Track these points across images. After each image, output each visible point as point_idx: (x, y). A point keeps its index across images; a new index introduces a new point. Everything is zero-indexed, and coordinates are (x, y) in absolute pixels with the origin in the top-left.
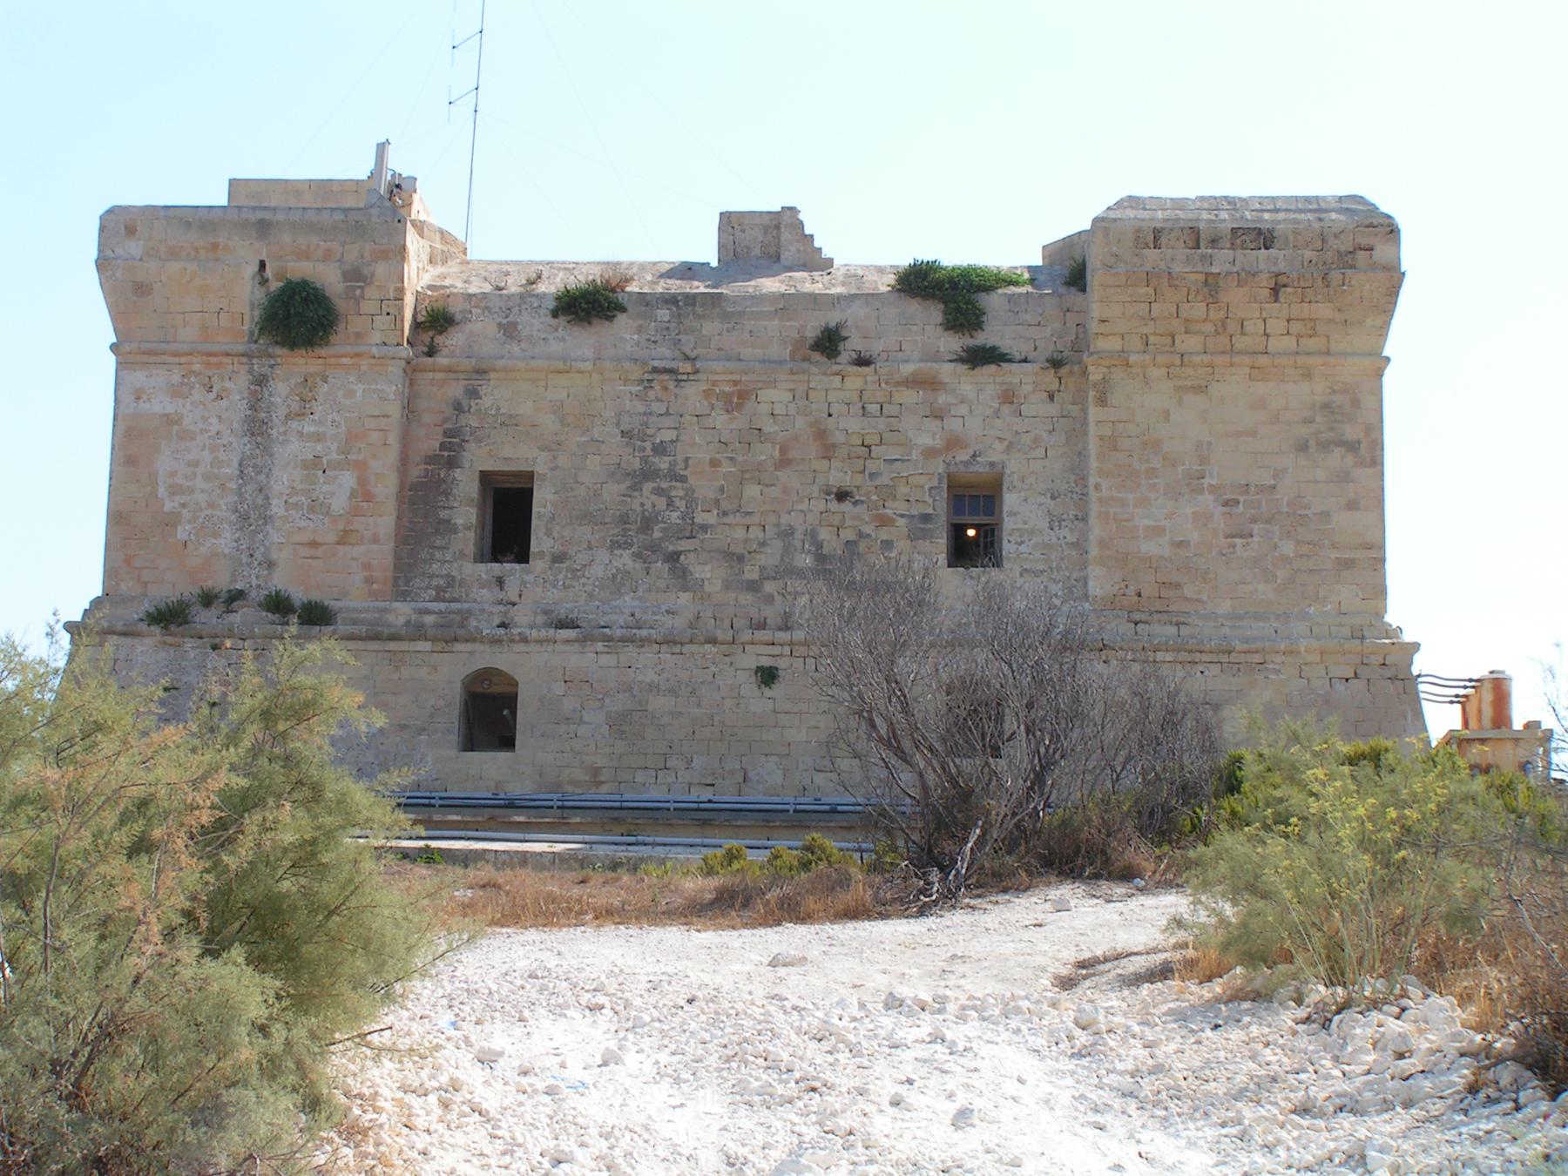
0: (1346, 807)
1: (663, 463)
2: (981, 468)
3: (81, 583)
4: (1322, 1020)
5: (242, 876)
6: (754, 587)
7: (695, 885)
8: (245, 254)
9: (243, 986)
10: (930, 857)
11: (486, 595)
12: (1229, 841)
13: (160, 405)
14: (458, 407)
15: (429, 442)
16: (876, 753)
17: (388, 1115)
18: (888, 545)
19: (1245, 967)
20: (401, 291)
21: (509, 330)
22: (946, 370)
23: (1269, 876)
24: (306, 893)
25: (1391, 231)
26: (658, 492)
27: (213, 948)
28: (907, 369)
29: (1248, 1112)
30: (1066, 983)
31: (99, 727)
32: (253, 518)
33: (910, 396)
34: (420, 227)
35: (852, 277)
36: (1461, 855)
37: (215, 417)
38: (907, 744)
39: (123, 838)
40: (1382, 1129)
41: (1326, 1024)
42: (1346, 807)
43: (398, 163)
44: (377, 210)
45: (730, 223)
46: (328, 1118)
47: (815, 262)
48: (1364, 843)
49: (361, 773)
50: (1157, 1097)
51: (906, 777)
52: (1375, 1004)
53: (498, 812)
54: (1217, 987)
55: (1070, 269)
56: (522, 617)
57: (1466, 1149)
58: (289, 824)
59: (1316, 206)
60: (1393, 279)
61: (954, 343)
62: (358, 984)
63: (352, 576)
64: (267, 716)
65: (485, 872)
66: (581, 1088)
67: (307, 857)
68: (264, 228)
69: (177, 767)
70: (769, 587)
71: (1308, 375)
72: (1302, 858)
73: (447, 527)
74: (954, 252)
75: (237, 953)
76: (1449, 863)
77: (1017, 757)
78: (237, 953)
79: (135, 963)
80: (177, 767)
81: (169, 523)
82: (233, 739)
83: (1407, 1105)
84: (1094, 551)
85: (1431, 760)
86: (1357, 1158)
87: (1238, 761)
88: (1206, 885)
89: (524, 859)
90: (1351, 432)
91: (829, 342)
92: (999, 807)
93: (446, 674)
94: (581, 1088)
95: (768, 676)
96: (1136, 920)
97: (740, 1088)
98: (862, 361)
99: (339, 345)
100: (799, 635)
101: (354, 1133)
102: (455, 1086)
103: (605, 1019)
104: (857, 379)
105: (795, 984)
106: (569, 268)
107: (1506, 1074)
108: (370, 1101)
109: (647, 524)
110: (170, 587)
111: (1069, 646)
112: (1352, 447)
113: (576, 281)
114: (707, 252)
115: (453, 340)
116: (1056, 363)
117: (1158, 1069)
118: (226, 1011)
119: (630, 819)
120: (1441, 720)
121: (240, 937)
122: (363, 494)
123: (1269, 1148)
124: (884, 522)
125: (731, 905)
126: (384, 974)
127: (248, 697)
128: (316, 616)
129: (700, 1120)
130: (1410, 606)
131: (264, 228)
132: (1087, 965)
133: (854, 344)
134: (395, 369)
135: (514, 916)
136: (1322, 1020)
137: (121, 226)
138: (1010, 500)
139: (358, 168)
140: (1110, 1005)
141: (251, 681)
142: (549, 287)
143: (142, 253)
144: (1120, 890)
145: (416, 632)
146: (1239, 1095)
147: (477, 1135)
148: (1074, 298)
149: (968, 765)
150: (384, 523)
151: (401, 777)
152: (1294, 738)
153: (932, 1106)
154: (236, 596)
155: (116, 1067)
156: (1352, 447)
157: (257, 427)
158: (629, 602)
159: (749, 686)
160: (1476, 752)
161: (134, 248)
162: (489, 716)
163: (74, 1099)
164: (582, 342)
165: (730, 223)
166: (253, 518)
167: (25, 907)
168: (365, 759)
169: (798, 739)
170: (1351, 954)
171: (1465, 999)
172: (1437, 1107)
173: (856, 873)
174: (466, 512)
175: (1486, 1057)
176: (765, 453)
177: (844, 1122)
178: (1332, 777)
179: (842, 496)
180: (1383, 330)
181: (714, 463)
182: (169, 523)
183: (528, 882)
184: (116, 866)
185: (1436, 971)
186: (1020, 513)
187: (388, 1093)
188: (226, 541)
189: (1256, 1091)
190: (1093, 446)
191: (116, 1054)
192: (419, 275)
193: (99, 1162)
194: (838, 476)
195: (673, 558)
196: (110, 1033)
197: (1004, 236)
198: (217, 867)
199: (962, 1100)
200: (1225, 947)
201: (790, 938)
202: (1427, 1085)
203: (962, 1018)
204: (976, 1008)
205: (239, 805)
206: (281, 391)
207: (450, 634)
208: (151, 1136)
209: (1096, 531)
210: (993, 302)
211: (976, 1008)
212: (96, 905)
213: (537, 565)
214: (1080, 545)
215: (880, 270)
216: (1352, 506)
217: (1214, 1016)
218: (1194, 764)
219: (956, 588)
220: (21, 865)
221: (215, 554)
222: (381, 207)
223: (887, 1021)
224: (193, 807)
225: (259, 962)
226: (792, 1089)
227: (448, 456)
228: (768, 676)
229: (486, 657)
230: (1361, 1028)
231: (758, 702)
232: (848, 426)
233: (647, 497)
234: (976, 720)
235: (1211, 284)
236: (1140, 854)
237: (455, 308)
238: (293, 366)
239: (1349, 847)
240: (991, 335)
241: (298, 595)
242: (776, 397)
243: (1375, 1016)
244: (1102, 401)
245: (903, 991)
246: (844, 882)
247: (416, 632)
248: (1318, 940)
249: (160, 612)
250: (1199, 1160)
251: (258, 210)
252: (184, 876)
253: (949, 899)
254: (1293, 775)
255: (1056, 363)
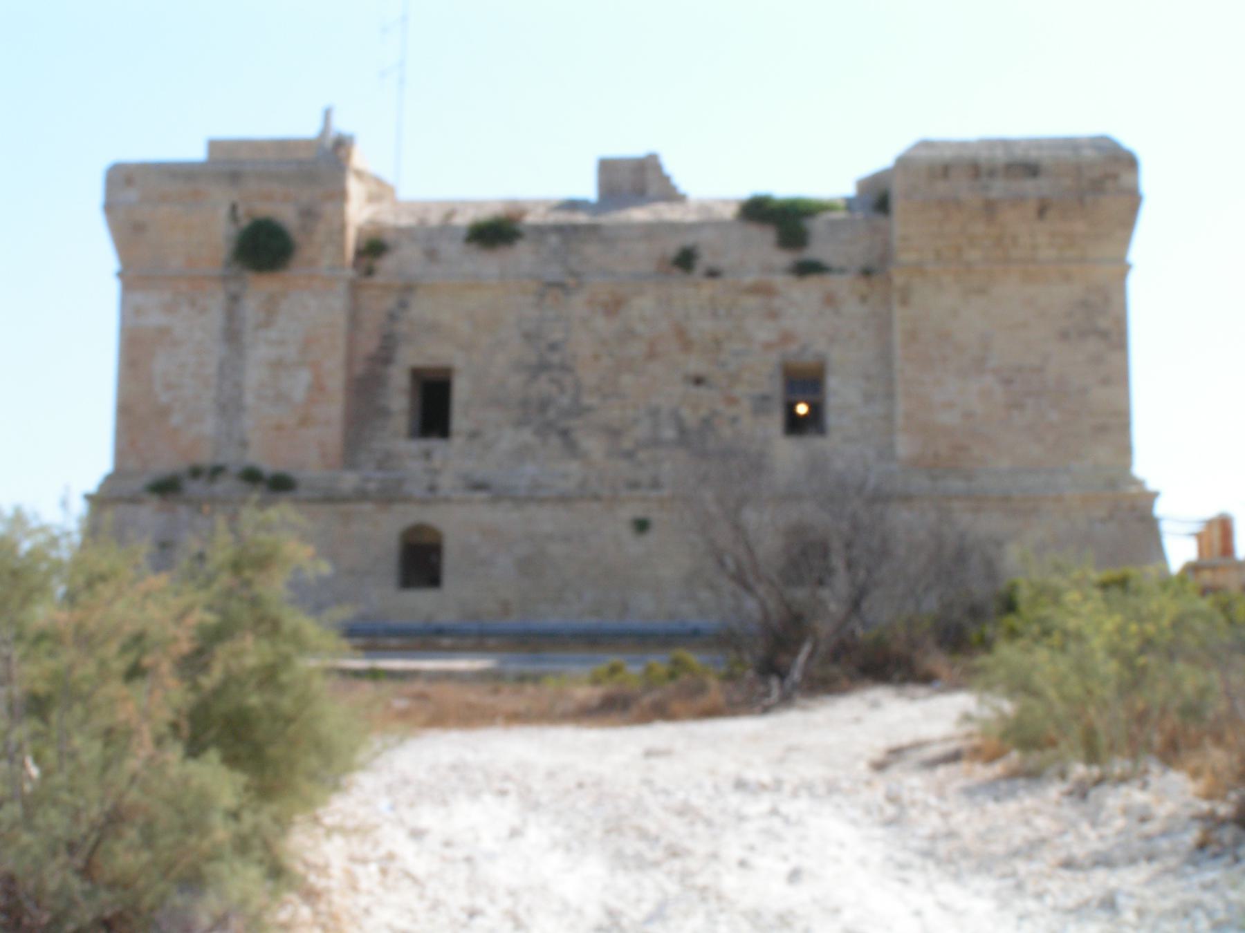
0: (1097, 623)
1: (555, 358)
2: (808, 359)
3: (94, 461)
4: (1081, 793)
5: (218, 693)
6: (629, 455)
7: (585, 693)
8: (220, 199)
9: (217, 780)
10: (771, 668)
11: (415, 467)
12: (1006, 651)
13: (155, 319)
14: (392, 317)
15: (369, 344)
16: (728, 586)
17: (334, 881)
18: (734, 420)
19: (1023, 750)
20: (342, 228)
21: (432, 255)
22: (781, 281)
23: (1038, 680)
24: (270, 707)
25: (1129, 162)
26: (553, 381)
27: (194, 749)
28: (749, 279)
29: (1022, 867)
30: (879, 766)
31: (103, 578)
32: (230, 407)
33: (752, 302)
34: (360, 174)
35: (704, 207)
36: (1191, 659)
37: (199, 327)
38: (751, 579)
39: (119, 665)
40: (1129, 880)
41: (1083, 795)
42: (1097, 623)
43: (341, 125)
44: (322, 164)
45: (608, 169)
46: (649, 753)
47: (671, 195)
48: (1113, 652)
49: (317, 609)
50: (948, 856)
51: (751, 605)
52: (1123, 780)
53: (428, 638)
54: (998, 768)
55: (877, 197)
56: (446, 482)
57: (1195, 895)
58: (250, 652)
59: (1073, 144)
60: (1132, 200)
61: (784, 258)
62: (312, 776)
63: (310, 451)
64: (236, 567)
65: (419, 686)
66: (491, 857)
67: (269, 676)
68: (235, 177)
69: (162, 608)
70: (642, 455)
71: (1067, 278)
72: (1064, 664)
73: (385, 413)
74: (784, 184)
75: (213, 755)
76: (1180, 667)
77: (841, 584)
78: (213, 755)
79: (133, 764)
80: (162, 608)
81: (164, 412)
82: (210, 580)
83: (1150, 858)
84: (900, 421)
85: (1166, 582)
86: (1109, 904)
87: (1014, 587)
88: (988, 687)
89: (449, 676)
90: (1103, 323)
91: (685, 260)
92: (824, 628)
93: (385, 529)
94: (491, 857)
95: (642, 526)
96: (932, 715)
97: (619, 855)
98: (713, 274)
99: (296, 271)
100: (666, 493)
101: (311, 895)
102: (391, 857)
103: (512, 803)
104: (708, 289)
105: (663, 770)
106: (478, 204)
107: (1228, 834)
108: (323, 870)
109: (544, 405)
110: (166, 463)
111: (880, 498)
112: (1104, 335)
113: (484, 215)
114: (586, 188)
115: (387, 264)
116: (867, 273)
117: (951, 835)
118: (204, 801)
119: (533, 641)
120: (1180, 551)
121: (217, 742)
122: (317, 387)
123: (1039, 896)
124: (732, 401)
125: (614, 708)
126: (332, 767)
127: (222, 551)
128: (281, 484)
129: (585, 881)
130: (1148, 465)
131: (235, 177)
132: (897, 753)
133: (706, 260)
134: (341, 288)
135: (440, 718)
136: (1081, 793)
137: (122, 179)
138: (833, 383)
139: (304, 127)
140: (913, 783)
141: (224, 537)
142: (463, 220)
143: (140, 201)
144: (921, 691)
145: (361, 495)
146: (1015, 853)
147: (408, 894)
148: (880, 220)
149: (800, 594)
150: (334, 409)
151: (345, 613)
152: (1058, 568)
153: (771, 867)
154: (217, 471)
155: (118, 847)
156: (1104, 335)
157: (232, 335)
158: (531, 468)
159: (627, 533)
160: (1207, 577)
161: (132, 195)
162: (421, 561)
163: (86, 872)
164: (489, 263)
165: (608, 169)
166: (230, 407)
167: (44, 719)
168: (314, 598)
169: (666, 576)
170: (1103, 741)
171: (1195, 774)
172: (1172, 862)
173: (713, 682)
174: (399, 400)
175: (1211, 821)
176: (636, 349)
177: (701, 880)
178: (1086, 598)
179: (699, 381)
180: (1125, 242)
181: (596, 357)
182: (164, 412)
183: (451, 694)
184: (115, 688)
185: (1172, 752)
186: (842, 392)
187: (338, 865)
188: (209, 426)
189: (1030, 849)
190: (898, 338)
191: (119, 836)
192: (359, 212)
193: (107, 924)
194: (696, 365)
195: (565, 434)
196: (115, 819)
197: (826, 175)
198: (195, 687)
199: (795, 861)
200: (1004, 736)
201: (660, 733)
202: (1164, 844)
203: (795, 794)
204: (807, 787)
205: (212, 637)
206: (251, 307)
207: (389, 496)
208: (148, 900)
209: (901, 406)
210: (816, 226)
211: (807, 787)
212: (101, 721)
213: (458, 441)
214: (889, 418)
215: (726, 202)
216: (1106, 381)
217: (992, 789)
218: (979, 590)
219: (788, 453)
220: (41, 687)
221: (198, 436)
222: (325, 162)
223: (735, 800)
224: (175, 639)
225: (232, 761)
226: (658, 854)
227: (384, 356)
228: (642, 526)
229: (411, 515)
230: (1114, 799)
231: (636, 547)
232: (702, 326)
233: (543, 386)
234: (807, 557)
235: (990, 208)
236: (936, 661)
237: (389, 238)
238: (260, 287)
239: (1100, 656)
240: (815, 251)
241: (268, 467)
242: (644, 304)
243: (1124, 789)
244: (905, 302)
245: (751, 775)
246: (701, 689)
247: (361, 495)
248: (1076, 731)
249: (157, 485)
250: (982, 906)
251: (231, 163)
252: (169, 695)
253: (786, 700)
254: (1056, 597)
255: (867, 273)
